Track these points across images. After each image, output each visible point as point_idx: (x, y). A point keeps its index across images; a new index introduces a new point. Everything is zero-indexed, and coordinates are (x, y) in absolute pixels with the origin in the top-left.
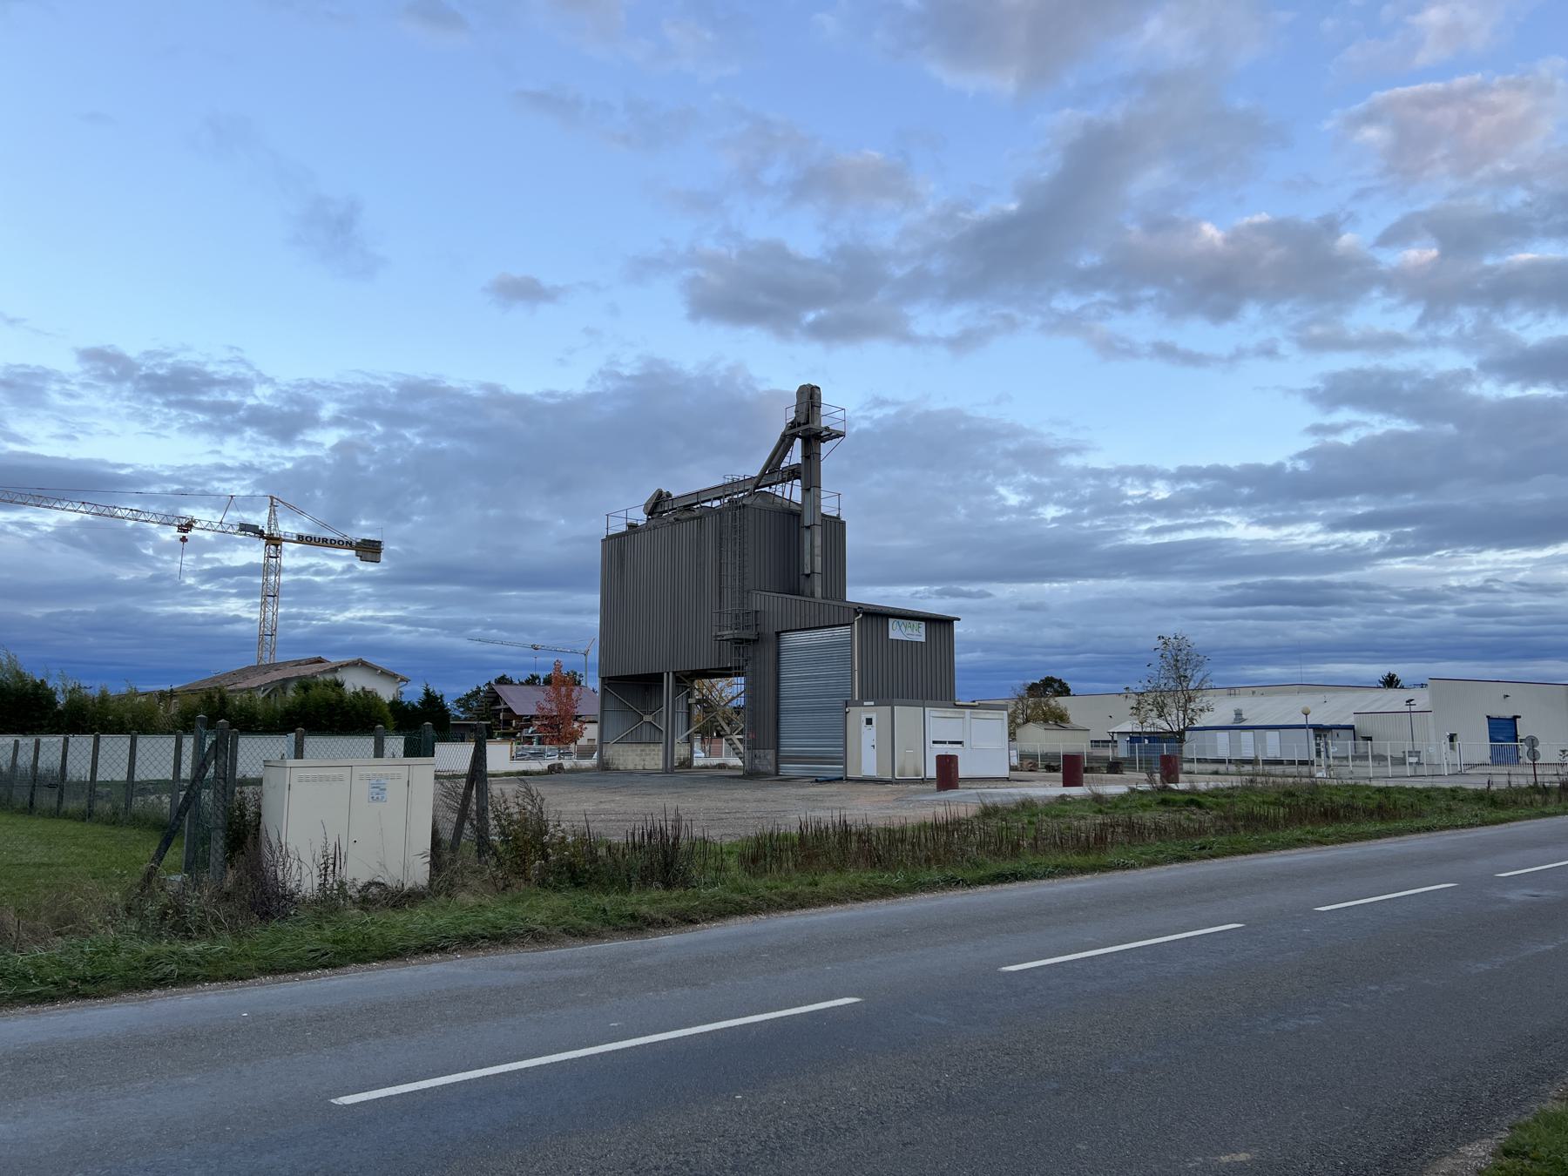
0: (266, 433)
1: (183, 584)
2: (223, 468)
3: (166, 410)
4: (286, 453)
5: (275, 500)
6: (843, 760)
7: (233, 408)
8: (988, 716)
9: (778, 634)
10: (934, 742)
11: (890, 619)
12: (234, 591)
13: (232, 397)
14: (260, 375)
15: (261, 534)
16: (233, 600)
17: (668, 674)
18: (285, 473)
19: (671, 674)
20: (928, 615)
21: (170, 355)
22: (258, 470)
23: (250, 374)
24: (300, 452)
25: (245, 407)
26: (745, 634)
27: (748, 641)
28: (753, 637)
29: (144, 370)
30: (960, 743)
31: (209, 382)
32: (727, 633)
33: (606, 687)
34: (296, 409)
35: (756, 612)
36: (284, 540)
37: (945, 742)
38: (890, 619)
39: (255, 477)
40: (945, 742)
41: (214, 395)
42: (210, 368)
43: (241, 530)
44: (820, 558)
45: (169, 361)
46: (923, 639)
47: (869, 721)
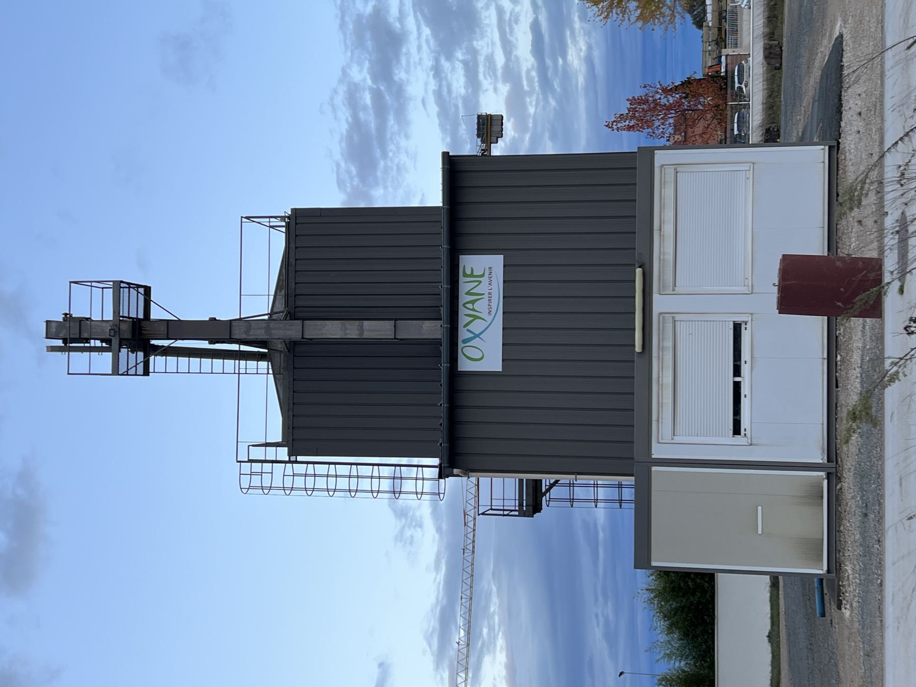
0: (398, 61)
1: (557, 108)
2: (438, 94)
3: (391, 154)
4: (413, 36)
7: (377, 96)
8: (669, 229)
10: (737, 430)
12: (560, 61)
13: (367, 99)
14: (341, 81)
16: (569, 58)
18: (435, 34)
21: (338, 165)
22: (437, 60)
23: (342, 89)
24: (411, 23)
25: (375, 87)
29: (356, 181)
30: (737, 328)
31: (356, 125)
34: (368, 35)
37: (737, 387)
39: (443, 60)
40: (737, 387)
41: (369, 118)
42: (344, 127)
45: (343, 164)
46: (496, 262)
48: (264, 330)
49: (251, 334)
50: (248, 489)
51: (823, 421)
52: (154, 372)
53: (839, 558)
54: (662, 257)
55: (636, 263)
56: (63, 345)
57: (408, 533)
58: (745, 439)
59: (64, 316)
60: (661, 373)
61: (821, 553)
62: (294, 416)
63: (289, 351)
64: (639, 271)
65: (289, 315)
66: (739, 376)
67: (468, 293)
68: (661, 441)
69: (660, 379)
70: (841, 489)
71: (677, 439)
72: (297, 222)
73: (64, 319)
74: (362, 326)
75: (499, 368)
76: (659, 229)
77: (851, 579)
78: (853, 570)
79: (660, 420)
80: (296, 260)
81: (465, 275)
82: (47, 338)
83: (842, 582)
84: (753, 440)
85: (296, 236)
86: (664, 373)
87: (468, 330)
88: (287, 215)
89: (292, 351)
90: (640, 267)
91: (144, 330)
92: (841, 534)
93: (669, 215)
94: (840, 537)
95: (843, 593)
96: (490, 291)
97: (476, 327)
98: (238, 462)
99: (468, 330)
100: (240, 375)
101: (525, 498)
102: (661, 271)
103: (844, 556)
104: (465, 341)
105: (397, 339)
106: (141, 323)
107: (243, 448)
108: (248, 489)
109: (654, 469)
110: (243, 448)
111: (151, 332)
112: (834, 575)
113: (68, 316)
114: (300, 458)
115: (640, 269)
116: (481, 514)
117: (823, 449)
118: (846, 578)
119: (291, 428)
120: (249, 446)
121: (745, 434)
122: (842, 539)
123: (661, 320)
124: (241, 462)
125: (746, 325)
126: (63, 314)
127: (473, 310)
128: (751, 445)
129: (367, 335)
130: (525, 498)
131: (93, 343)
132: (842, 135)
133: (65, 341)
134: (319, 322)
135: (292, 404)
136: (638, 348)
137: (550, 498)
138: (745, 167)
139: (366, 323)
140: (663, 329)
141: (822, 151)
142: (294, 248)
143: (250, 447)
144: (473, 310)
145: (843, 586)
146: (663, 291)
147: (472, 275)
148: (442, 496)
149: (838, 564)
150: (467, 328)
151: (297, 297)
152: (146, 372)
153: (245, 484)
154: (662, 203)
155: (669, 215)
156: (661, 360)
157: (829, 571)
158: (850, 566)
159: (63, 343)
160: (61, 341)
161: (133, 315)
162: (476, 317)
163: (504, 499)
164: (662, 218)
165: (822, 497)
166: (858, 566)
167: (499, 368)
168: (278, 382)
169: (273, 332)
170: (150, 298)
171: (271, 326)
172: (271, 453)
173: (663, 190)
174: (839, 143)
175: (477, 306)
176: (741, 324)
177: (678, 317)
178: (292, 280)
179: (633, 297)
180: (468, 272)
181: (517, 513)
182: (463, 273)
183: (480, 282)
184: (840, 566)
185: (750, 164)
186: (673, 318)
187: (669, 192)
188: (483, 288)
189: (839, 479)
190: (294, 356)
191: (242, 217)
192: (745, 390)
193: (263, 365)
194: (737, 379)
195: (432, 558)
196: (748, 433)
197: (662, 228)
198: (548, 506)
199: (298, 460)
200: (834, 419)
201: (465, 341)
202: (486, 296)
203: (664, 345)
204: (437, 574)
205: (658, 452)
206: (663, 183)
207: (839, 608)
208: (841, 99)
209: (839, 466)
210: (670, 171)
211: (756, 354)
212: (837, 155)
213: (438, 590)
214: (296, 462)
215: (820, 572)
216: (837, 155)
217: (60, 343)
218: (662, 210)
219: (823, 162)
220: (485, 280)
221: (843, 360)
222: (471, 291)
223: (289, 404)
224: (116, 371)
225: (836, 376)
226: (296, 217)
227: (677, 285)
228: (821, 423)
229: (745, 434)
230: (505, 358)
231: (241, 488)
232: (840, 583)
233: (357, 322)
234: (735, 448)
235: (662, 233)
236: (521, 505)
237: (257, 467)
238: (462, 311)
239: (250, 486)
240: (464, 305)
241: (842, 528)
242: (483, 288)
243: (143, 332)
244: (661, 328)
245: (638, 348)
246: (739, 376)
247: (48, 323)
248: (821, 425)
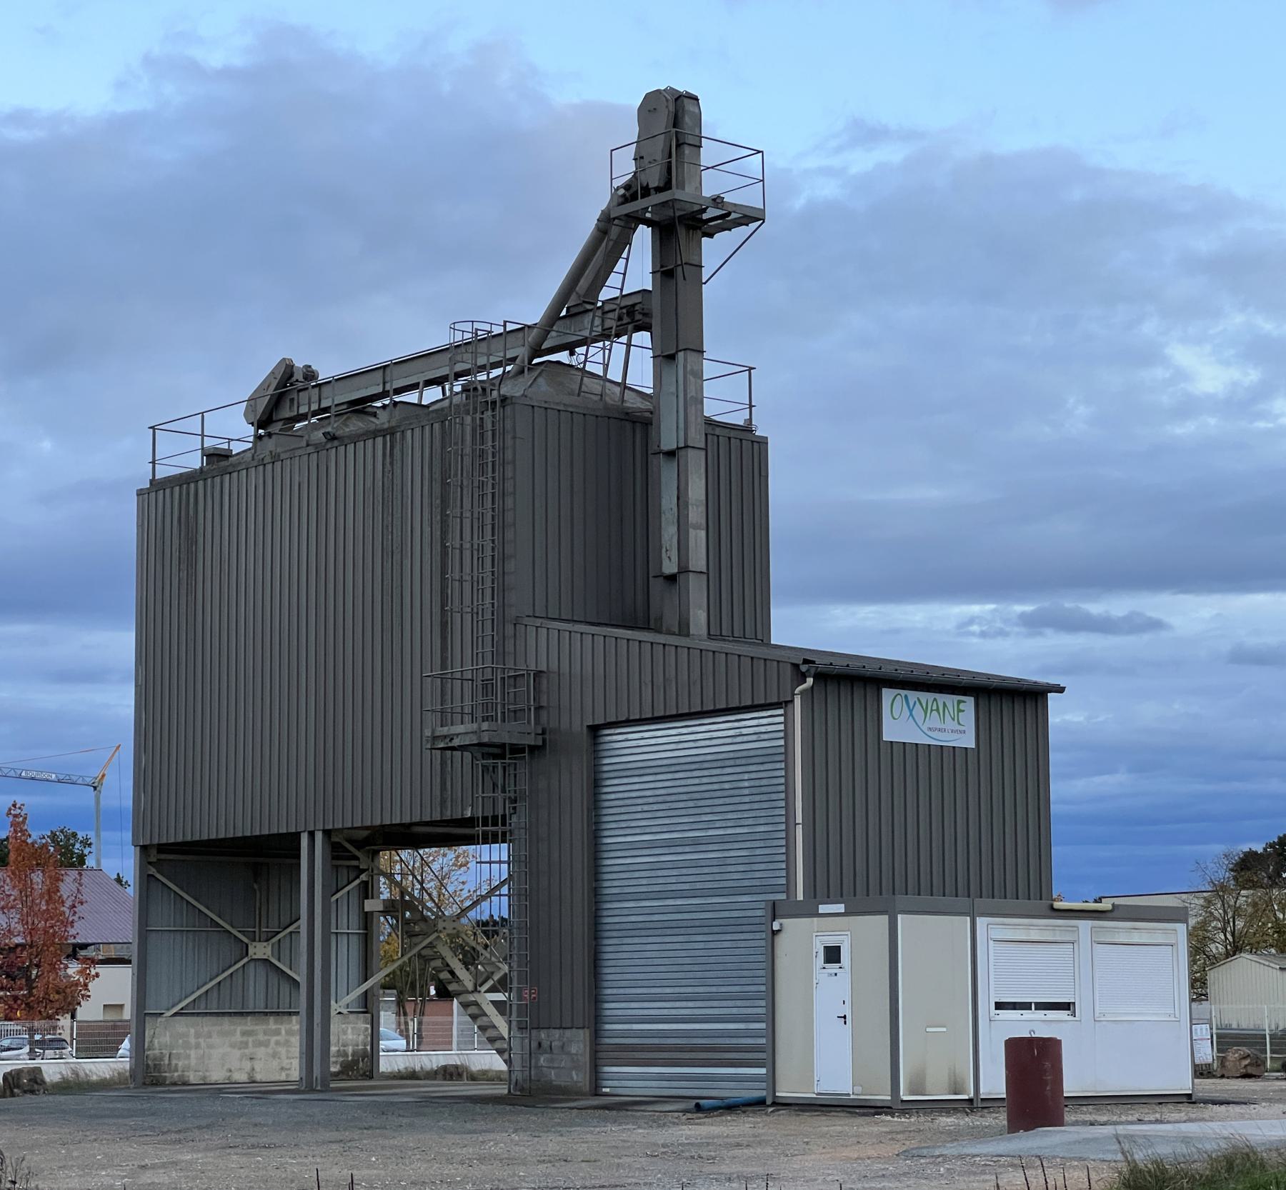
6: (766, 1054)
9: (595, 730)
10: (999, 1006)
17: (312, 835)
19: (319, 836)
26: (508, 733)
27: (516, 750)
28: (530, 741)
30: (1066, 1006)
32: (463, 731)
33: (152, 871)
35: (538, 674)
37: (1025, 1006)
40: (1025, 1006)
47: (833, 955)
68: (990, 926)
71: (991, 943)
75: (886, 737)
81: (959, 702)
87: (915, 703)
89: (627, 417)
109: (968, 918)
117: (990, 1094)
119: (546, 406)
129: (692, 532)
134: (703, 470)
139: (703, 533)
144: (932, 710)
147: (959, 711)
155: (1145, 938)
157: (902, 1101)
165: (956, 1094)
167: (886, 737)
169: (693, 407)
202: (943, 726)
205: (981, 922)
215: (901, 1094)
220: (954, 725)
230: (894, 744)
233: (704, 522)
234: (987, 1007)
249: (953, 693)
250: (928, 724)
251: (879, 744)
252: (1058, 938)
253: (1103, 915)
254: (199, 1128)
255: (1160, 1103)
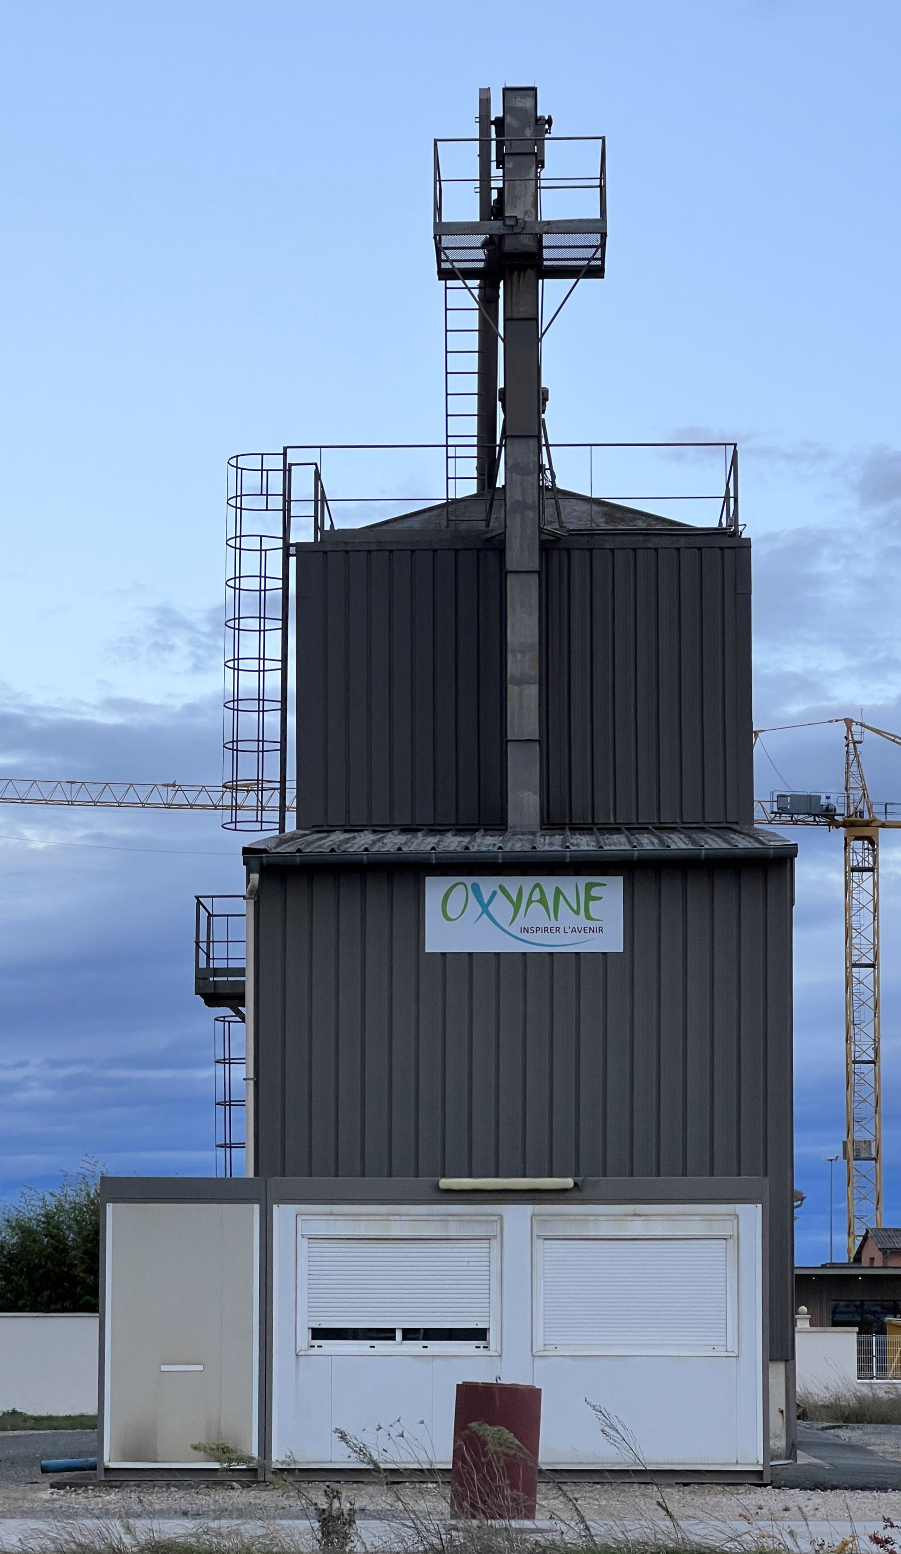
5: (855, 728)
8: (636, 1228)
10: (319, 1334)
11: (429, 880)
15: (828, 816)
20: (540, 860)
30: (479, 1334)
36: (883, 826)
37: (387, 1334)
38: (429, 880)
40: (387, 1334)
43: (782, 811)
44: (533, 690)
48: (521, 499)
49: (514, 474)
50: (237, 467)
51: (336, 1462)
52: (446, 288)
53: (127, 1486)
54: (592, 1218)
55: (582, 1178)
56: (493, 119)
57: (179, 639)
58: (305, 1346)
59: (547, 118)
60: (407, 1218)
61: (136, 1460)
62: (369, 552)
63: (489, 540)
64: (569, 1182)
65: (553, 538)
66: (405, 1338)
67: (558, 892)
68: (300, 1218)
69: (397, 1218)
70: (233, 1488)
71: (303, 1243)
72: (726, 550)
73: (542, 118)
74: (528, 683)
76: (637, 1213)
77: (96, 1499)
78: (110, 1502)
79: (332, 1218)
80: (656, 549)
81: (589, 887)
82: (505, 90)
83: (92, 1490)
84: (304, 1357)
85: (700, 549)
86: (438, 1223)
87: (495, 893)
88: (740, 528)
90: (575, 1184)
91: (519, 278)
92: (164, 1489)
93: (659, 1228)
94: (160, 1487)
95: (75, 1490)
96: (562, 930)
97: (501, 908)
98: (285, 449)
99: (495, 893)
100: (449, 444)
101: (231, 979)
102: (568, 1218)
103: (131, 1492)
104: (476, 888)
105: (506, 745)
106: (532, 269)
107: (312, 456)
108: (237, 467)
109: (256, 1207)
110: (312, 456)
111: (514, 289)
112: (103, 1479)
113: (547, 126)
114: (293, 561)
115: (572, 1185)
116: (199, 901)
118: (98, 1494)
119: (348, 548)
120: (316, 464)
121: (314, 1346)
122: (157, 1488)
123: (491, 1218)
124: (285, 454)
125: (484, 1347)
126: (550, 117)
127: (530, 902)
128: (297, 1355)
129: (512, 690)
130: (231, 979)
131: (496, 172)
132: (777, 1490)
133: (499, 122)
135: (391, 548)
136: (445, 1183)
137: (229, 1022)
138: (732, 1345)
140: (476, 1221)
141: (756, 1462)
142: (678, 546)
143: (314, 467)
144: (530, 902)
145: (86, 1491)
146: (538, 1221)
147: (589, 898)
148: (232, 826)
149: (118, 1483)
150: (499, 892)
151: (588, 554)
152: (445, 274)
153: (243, 462)
154: (678, 1218)
155: (659, 1228)
156: (425, 1218)
157: (108, 1470)
158: (115, 1498)
159: (497, 119)
160: (501, 115)
161: (546, 253)
162: (517, 908)
163: (228, 942)
164: (654, 1218)
166: (113, 1506)
167: (433, 945)
168: (435, 512)
170: (583, 278)
171: (528, 512)
172: (303, 511)
173: (698, 1218)
174: (765, 1485)
175: (537, 907)
176: (485, 1339)
177: (495, 1244)
178: (619, 541)
179: (525, 1173)
180: (594, 892)
181: (203, 965)
182: (593, 883)
183: (577, 913)
184: (116, 1487)
185: (736, 1351)
186: (495, 1237)
187: (695, 1228)
188: (566, 917)
189: (246, 1486)
190: (479, 550)
191: (735, 445)
192: (382, 1346)
193: (470, 488)
194: (399, 1335)
195: (126, 691)
196: (316, 1351)
197: (638, 1218)
198: (216, 1019)
199: (291, 558)
200: (339, 1480)
201: (476, 888)
202: (553, 923)
203: (452, 1223)
204: (96, 707)
205: (281, 1213)
206: (709, 1217)
207: (52, 1486)
208: (836, 1488)
209: (267, 1486)
210: (727, 1230)
211: (438, 1363)
212: (749, 1484)
213: (58, 710)
214: (286, 557)
215: (106, 1457)
216: (749, 1484)
217: (496, 111)
218: (665, 1218)
219: (737, 1463)
220: (581, 921)
221: (427, 1490)
222: (561, 897)
223: (392, 542)
224: (441, 230)
225: (405, 1482)
226: (734, 548)
227: (546, 1242)
228: (333, 1460)
229: (314, 1346)
230: (448, 957)
231: (237, 456)
232: (90, 1487)
235: (629, 1218)
236: (216, 972)
237: (276, 483)
238: (527, 883)
239: (242, 469)
240: (537, 885)
241: (172, 1489)
242: (566, 917)
243: (516, 273)
244: (478, 1218)
245: (445, 1183)
246: (405, 1338)
247: (532, 92)
248: (329, 1460)
249: (577, 874)
250: (520, 921)
251: (418, 959)
252: (453, 1234)
253: (561, 1196)
254: (589, 1483)
255: (685, 1485)
